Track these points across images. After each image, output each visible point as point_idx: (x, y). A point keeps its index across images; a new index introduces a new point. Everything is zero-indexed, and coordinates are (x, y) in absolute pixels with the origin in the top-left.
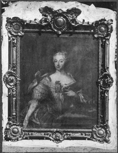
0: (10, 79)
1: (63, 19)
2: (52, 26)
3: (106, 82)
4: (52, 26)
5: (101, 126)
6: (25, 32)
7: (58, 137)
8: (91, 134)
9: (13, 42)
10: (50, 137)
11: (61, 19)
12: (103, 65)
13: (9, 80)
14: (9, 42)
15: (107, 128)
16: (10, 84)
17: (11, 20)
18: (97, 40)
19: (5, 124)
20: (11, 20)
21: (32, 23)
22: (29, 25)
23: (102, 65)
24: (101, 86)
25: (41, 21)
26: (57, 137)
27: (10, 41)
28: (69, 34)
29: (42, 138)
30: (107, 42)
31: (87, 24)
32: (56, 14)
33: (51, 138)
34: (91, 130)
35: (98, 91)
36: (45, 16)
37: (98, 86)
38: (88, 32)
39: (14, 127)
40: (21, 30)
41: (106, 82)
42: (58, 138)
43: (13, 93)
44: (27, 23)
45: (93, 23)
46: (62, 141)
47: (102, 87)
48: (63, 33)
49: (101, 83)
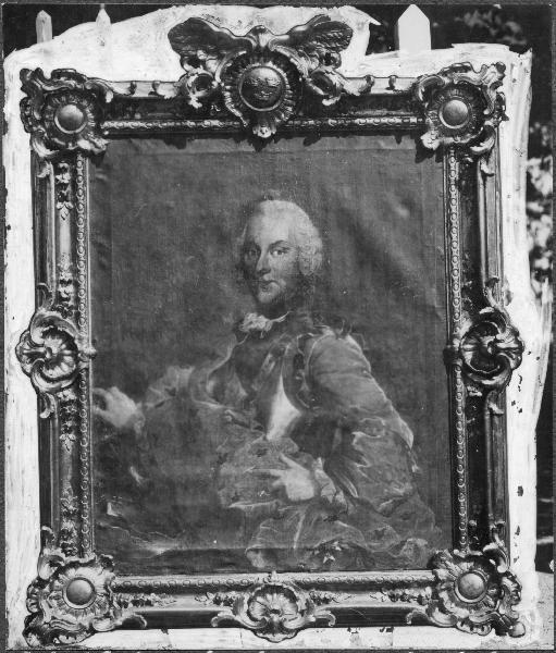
0: (50, 350)
1: (278, 74)
2: (227, 94)
3: (490, 350)
4: (227, 94)
5: (469, 558)
6: (115, 134)
7: (276, 612)
8: (429, 591)
9: (57, 180)
10: (237, 618)
11: (269, 74)
12: (473, 269)
13: (43, 355)
14: (40, 420)
15: (498, 564)
16: (50, 371)
17: (48, 82)
18: (439, 160)
19: (24, 564)
20: (48, 82)
21: (138, 94)
22: (126, 104)
23: (467, 275)
24: (465, 369)
25: (182, 92)
26: (272, 615)
27: (44, 415)
28: (302, 140)
29: (201, 621)
30: (484, 167)
31: (388, 89)
32: (243, 53)
33: (242, 618)
34: (428, 575)
35: (453, 391)
36: (195, 62)
37: (451, 368)
38: (394, 125)
39: (72, 573)
40: (94, 124)
41: (490, 350)
42: (276, 618)
43: (59, 177)
44: (117, 98)
45: (415, 86)
46: (298, 630)
47: (471, 371)
48: (284, 133)
49: (469, 356)
